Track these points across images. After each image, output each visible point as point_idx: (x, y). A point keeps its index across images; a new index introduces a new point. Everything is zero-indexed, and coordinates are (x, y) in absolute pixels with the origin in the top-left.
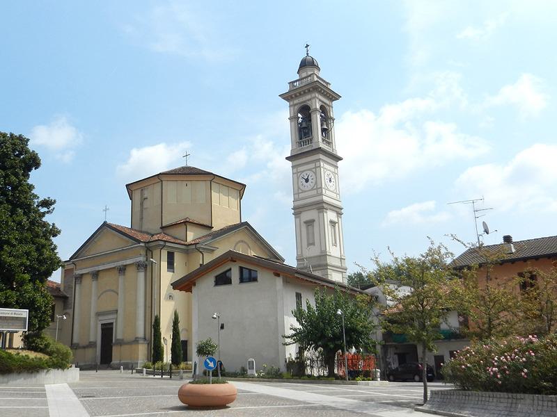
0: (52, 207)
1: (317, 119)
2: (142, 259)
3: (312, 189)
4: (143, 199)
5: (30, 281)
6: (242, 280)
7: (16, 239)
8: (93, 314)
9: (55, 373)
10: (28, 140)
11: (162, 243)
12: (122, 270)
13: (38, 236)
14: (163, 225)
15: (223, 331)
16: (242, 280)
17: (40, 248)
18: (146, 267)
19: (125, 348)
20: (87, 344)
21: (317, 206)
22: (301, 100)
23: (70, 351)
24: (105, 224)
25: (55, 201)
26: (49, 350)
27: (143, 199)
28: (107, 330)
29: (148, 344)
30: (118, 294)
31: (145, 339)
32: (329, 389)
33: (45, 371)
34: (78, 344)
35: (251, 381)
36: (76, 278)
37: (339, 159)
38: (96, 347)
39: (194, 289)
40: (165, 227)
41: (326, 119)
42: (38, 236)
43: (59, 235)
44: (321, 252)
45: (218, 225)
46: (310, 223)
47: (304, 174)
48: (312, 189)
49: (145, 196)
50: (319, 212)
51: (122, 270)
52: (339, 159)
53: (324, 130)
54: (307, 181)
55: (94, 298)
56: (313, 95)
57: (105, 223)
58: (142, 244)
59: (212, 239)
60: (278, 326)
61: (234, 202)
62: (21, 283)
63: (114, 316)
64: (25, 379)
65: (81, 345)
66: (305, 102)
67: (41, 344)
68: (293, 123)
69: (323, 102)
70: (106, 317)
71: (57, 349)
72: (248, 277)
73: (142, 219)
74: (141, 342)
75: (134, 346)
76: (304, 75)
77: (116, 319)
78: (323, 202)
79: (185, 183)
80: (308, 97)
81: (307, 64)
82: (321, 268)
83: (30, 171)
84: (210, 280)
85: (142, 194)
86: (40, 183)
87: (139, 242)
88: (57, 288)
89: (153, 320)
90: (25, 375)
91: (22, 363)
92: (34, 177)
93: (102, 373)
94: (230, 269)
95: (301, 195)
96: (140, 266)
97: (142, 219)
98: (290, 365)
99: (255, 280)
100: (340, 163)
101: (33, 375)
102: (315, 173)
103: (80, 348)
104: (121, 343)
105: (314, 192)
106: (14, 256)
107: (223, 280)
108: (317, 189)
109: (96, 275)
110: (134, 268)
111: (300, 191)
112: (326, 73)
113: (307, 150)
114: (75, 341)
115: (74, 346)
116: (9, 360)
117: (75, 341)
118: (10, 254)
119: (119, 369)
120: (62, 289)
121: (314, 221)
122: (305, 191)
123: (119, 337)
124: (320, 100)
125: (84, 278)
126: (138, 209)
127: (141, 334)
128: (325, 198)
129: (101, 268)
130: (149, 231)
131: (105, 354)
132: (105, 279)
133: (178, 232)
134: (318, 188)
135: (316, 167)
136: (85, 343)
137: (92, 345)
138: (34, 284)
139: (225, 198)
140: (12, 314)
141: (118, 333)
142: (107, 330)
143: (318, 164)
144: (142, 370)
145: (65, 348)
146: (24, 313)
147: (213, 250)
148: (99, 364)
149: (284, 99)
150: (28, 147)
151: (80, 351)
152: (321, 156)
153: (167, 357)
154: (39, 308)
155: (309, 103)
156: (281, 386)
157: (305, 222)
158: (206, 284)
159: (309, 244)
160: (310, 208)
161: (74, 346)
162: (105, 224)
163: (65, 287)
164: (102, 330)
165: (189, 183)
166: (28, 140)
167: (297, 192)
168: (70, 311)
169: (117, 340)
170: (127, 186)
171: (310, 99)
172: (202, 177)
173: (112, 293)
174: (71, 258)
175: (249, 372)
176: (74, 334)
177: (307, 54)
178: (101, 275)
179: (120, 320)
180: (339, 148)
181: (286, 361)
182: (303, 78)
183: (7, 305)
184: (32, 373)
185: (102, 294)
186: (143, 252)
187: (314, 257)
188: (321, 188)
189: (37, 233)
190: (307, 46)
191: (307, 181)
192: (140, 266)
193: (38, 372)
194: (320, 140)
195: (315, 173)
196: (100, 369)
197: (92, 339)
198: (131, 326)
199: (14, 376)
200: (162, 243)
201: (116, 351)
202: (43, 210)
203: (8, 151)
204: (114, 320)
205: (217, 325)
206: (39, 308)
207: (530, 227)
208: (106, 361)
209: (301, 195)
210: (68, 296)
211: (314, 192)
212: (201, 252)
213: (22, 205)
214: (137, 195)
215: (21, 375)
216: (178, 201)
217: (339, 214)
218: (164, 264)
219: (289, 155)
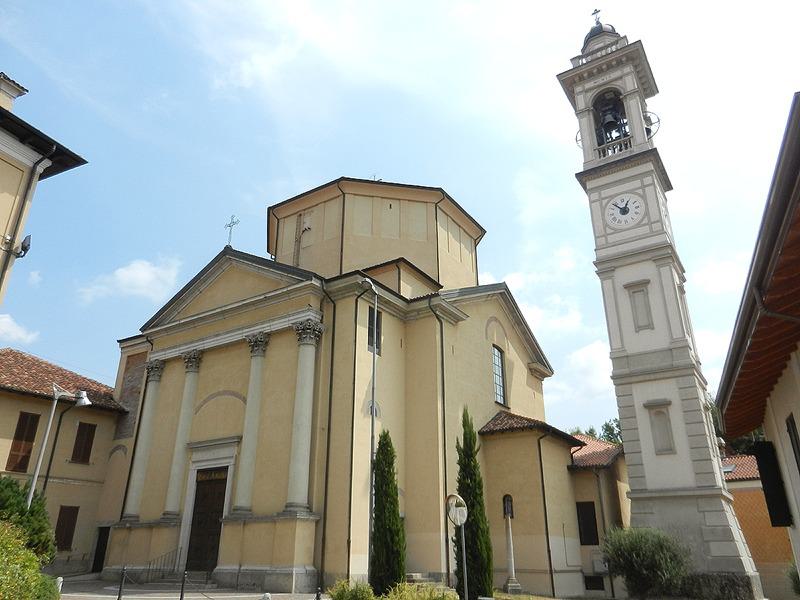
2: (312, 316)
3: (639, 225)
4: (302, 231)
8: (180, 447)
12: (259, 344)
18: (318, 337)
19: (257, 533)
20: (159, 515)
21: (653, 254)
22: (600, 81)
24: (228, 250)
27: (302, 231)
28: (211, 486)
29: (317, 522)
30: (245, 400)
31: (309, 508)
36: (151, 369)
38: (178, 525)
44: (673, 341)
46: (637, 287)
47: (617, 200)
48: (639, 225)
49: (306, 226)
50: (659, 266)
54: (624, 211)
55: (185, 411)
63: (231, 451)
65: (259, 510)
68: (585, 120)
74: (302, 515)
77: (237, 458)
82: (677, 373)
88: (106, 394)
89: (376, 446)
104: (245, 517)
105: (645, 230)
108: (650, 223)
110: (293, 337)
120: (116, 397)
121: (647, 282)
122: (622, 230)
127: (300, 496)
132: (213, 367)
135: (643, 187)
136: (155, 514)
137: (170, 520)
139: (455, 244)
141: (241, 493)
142: (211, 486)
148: (182, 568)
150: (120, 270)
155: (618, 84)
157: (627, 287)
159: (638, 328)
160: (628, 261)
162: (228, 250)
163: (123, 391)
165: (395, 204)
168: (128, 442)
171: (621, 78)
173: (232, 398)
178: (207, 360)
185: (205, 401)
186: (315, 302)
187: (661, 351)
192: (303, 332)
197: (171, 507)
201: (229, 538)
204: (232, 461)
210: (127, 409)
211: (645, 230)
212: (438, 317)
218: (363, 332)
219: (582, 170)
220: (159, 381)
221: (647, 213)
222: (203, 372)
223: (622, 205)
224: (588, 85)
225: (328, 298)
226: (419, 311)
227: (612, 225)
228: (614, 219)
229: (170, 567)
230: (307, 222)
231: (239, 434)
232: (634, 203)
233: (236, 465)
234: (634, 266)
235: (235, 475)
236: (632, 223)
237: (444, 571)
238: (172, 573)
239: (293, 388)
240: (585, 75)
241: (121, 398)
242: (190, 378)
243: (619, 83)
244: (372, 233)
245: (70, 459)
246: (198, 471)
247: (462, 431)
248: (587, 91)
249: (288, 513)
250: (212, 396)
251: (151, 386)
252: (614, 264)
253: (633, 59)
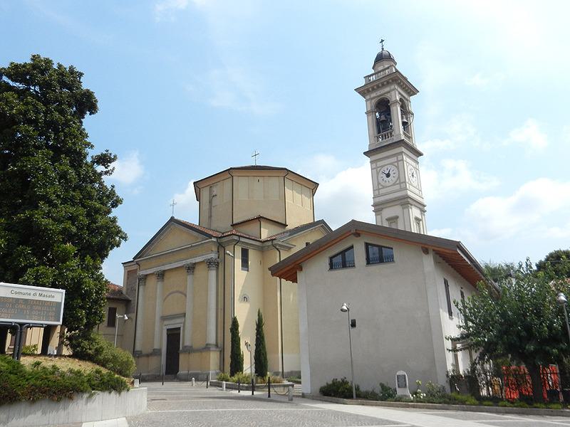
0: (112, 165)
1: (396, 111)
2: (213, 256)
3: (394, 184)
4: (212, 197)
5: (76, 255)
6: (369, 262)
7: (58, 196)
9: (103, 400)
10: (81, 74)
11: (236, 238)
12: (191, 268)
13: (91, 198)
14: (234, 223)
15: (354, 329)
16: (369, 262)
17: (92, 213)
19: (194, 358)
22: (379, 93)
23: (132, 359)
25: (115, 156)
26: (101, 357)
27: (212, 197)
28: (174, 336)
29: (221, 351)
30: (186, 296)
31: (217, 345)
32: (514, 419)
33: (86, 395)
34: (141, 351)
35: (414, 407)
38: (160, 354)
39: (300, 276)
40: (236, 224)
41: (405, 112)
42: (91, 198)
43: (119, 206)
45: (292, 223)
48: (394, 184)
49: (214, 194)
50: (403, 208)
51: (191, 268)
52: (419, 154)
53: (405, 124)
54: (388, 175)
55: (159, 301)
56: (392, 87)
57: (172, 218)
58: (214, 240)
59: (290, 235)
60: (431, 330)
61: (307, 200)
62: (65, 258)
64: (44, 413)
67: (90, 349)
69: (402, 95)
70: (172, 322)
71: (114, 356)
72: (378, 256)
73: (210, 217)
75: (204, 354)
76: (381, 68)
77: (184, 323)
78: (409, 197)
80: (387, 89)
81: (382, 58)
83: (83, 118)
84: (323, 262)
85: (211, 192)
86: (97, 131)
87: (210, 236)
90: (45, 404)
91: (39, 383)
92: (89, 122)
93: (168, 385)
94: (352, 247)
95: (382, 191)
96: (210, 263)
97: (210, 217)
98: (455, 379)
99: (390, 259)
101: (61, 405)
102: (397, 167)
103: (143, 356)
104: (189, 350)
105: (397, 187)
106: (54, 219)
107: (342, 261)
108: (400, 183)
109: (161, 275)
110: (204, 266)
111: (380, 187)
112: (402, 67)
113: (386, 144)
114: (138, 348)
115: (137, 354)
116: (12, 376)
117: (138, 348)
118: (48, 215)
119: (191, 380)
120: (124, 292)
121: (397, 217)
122: (387, 187)
123: (187, 343)
124: (400, 93)
125: (148, 278)
126: (206, 207)
127: (212, 340)
128: (409, 193)
129: (167, 267)
130: (218, 229)
131: (171, 363)
132: (172, 280)
133: (250, 230)
134: (401, 183)
135: (398, 161)
136: (148, 350)
137: (156, 353)
138: (83, 260)
139: (298, 196)
140: (35, 295)
141: (187, 339)
142: (174, 336)
143: (400, 157)
144: (222, 384)
145: (125, 355)
146: (59, 296)
147: (291, 248)
151: (143, 360)
152: (404, 150)
153: (248, 367)
154: (89, 293)
155: (388, 96)
156: (376, 405)
158: (318, 269)
161: (137, 354)
162: (172, 218)
163: (127, 289)
164: (168, 336)
165: (261, 179)
166: (81, 74)
167: (377, 188)
169: (186, 347)
171: (389, 92)
172: (275, 173)
173: (180, 295)
174: (134, 258)
175: (400, 392)
176: (137, 332)
177: (383, 49)
178: (167, 275)
179: (188, 324)
181: (447, 376)
182: (380, 72)
183: (15, 276)
184: (59, 400)
186: (215, 249)
188: (405, 182)
189: (89, 193)
190: (382, 41)
191: (388, 175)
192: (210, 263)
193: (71, 398)
194: (402, 133)
195: (397, 167)
196: (167, 380)
197: (156, 346)
198: (201, 330)
199: (22, 407)
200: (236, 238)
201: (183, 359)
202: (100, 168)
203: (51, 80)
204: (182, 325)
205: (348, 323)
206: (89, 293)
207: (565, 248)
208: (171, 371)
209: (382, 191)
211: (397, 187)
212: (277, 249)
213: (69, 152)
214: (205, 194)
215: (38, 405)
217: (423, 211)
218: (238, 262)
220: (145, 285)
221: (399, 177)
222: (165, 281)
223: (387, 172)
224: (373, 95)
225: (221, 246)
226: (268, 246)
227: (382, 183)
228: (383, 180)
229: (158, 374)
230: (215, 190)
231: (182, 312)
232: (393, 170)
233: (184, 327)
234: (390, 208)
235: (184, 330)
236: (391, 183)
237: (281, 370)
238: (159, 376)
239: (207, 291)
240: (370, 89)
241: (127, 293)
242: (160, 284)
243: (388, 95)
244: (249, 198)
245: (118, 395)
246: (168, 330)
247: (257, 317)
248: (372, 99)
249: (207, 348)
250: (170, 294)
251: (141, 288)
252: (382, 206)
253: (396, 80)
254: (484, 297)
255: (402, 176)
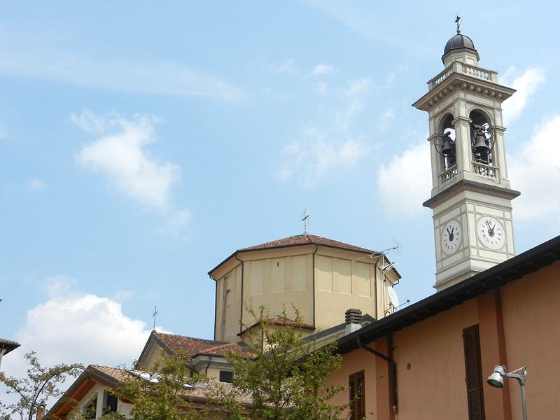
3: (458, 251)
37: (513, 195)
48: (458, 251)
52: (513, 195)
56: (456, 96)
66: (446, 109)
79: (276, 261)
80: (450, 101)
81: (457, 46)
100: (514, 202)
102: (461, 224)
105: (460, 256)
135: (462, 214)
143: (463, 207)
149: (420, 108)
152: (468, 194)
165: (281, 262)
170: (210, 273)
172: (363, 258)
177: (458, 32)
180: (512, 172)
190: (458, 18)
200: (205, 359)
209: (446, 263)
211: (460, 256)
216: (268, 292)
221: (462, 241)
254: (301, 344)
255: (438, 235)
